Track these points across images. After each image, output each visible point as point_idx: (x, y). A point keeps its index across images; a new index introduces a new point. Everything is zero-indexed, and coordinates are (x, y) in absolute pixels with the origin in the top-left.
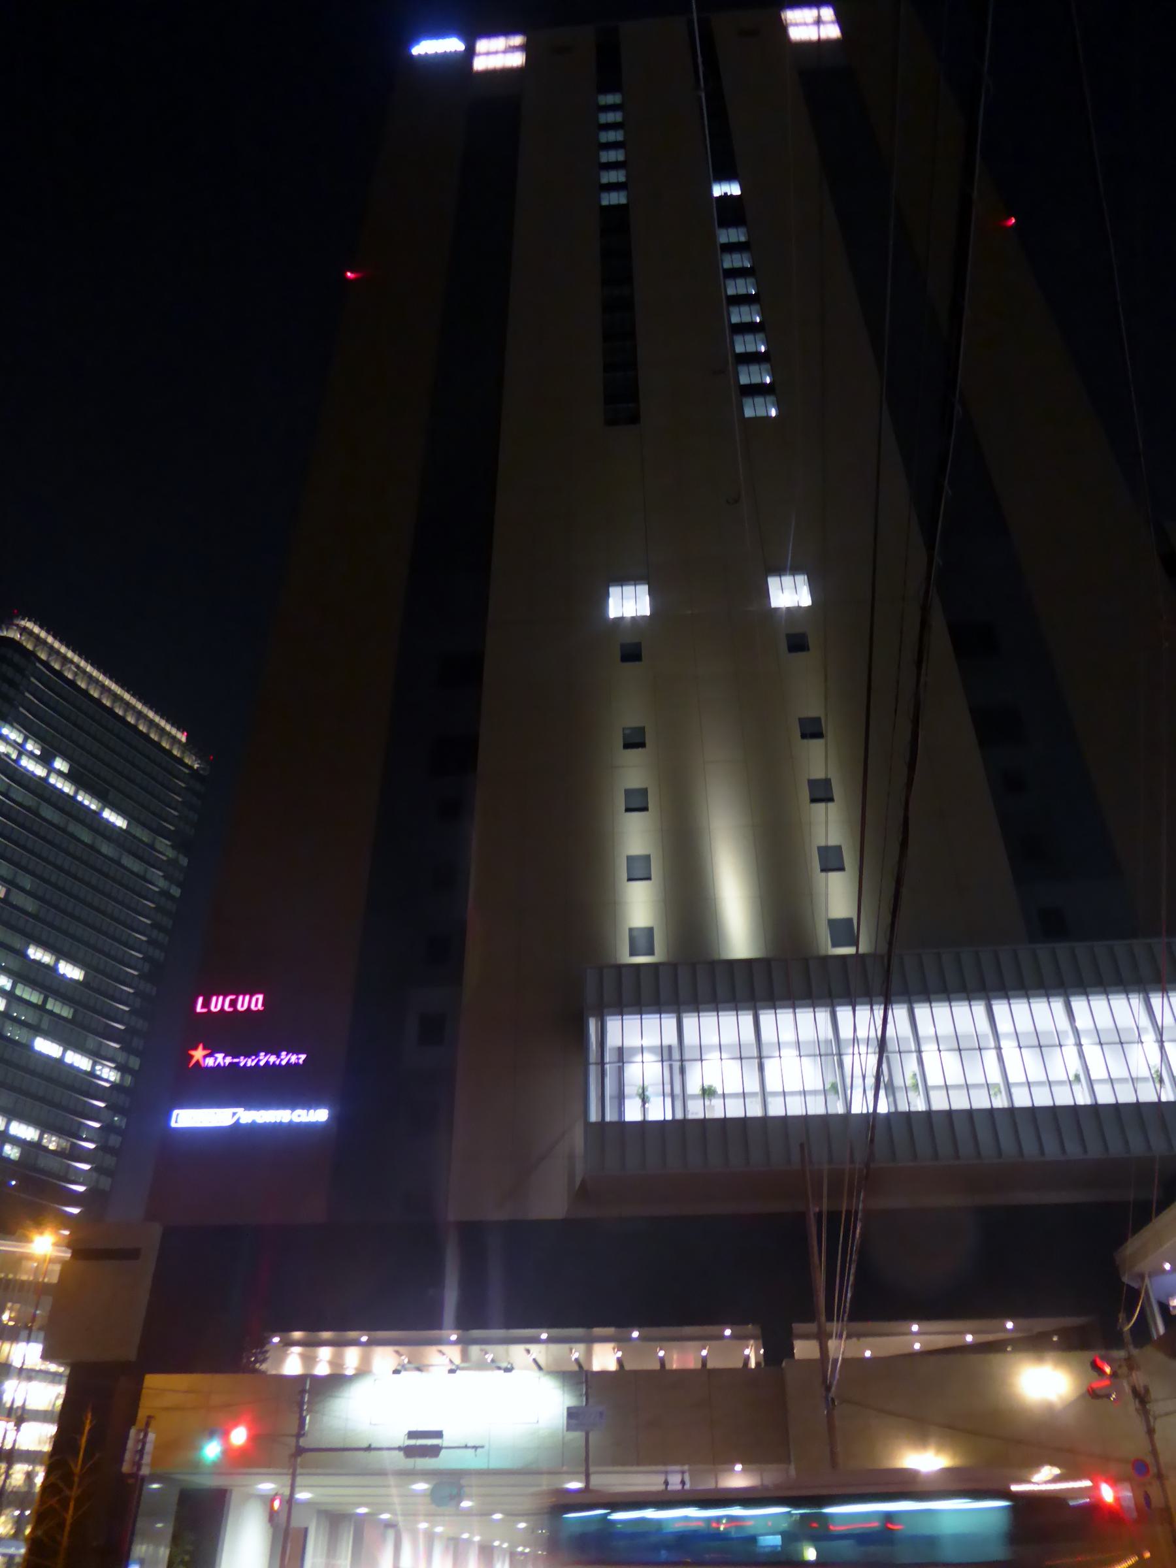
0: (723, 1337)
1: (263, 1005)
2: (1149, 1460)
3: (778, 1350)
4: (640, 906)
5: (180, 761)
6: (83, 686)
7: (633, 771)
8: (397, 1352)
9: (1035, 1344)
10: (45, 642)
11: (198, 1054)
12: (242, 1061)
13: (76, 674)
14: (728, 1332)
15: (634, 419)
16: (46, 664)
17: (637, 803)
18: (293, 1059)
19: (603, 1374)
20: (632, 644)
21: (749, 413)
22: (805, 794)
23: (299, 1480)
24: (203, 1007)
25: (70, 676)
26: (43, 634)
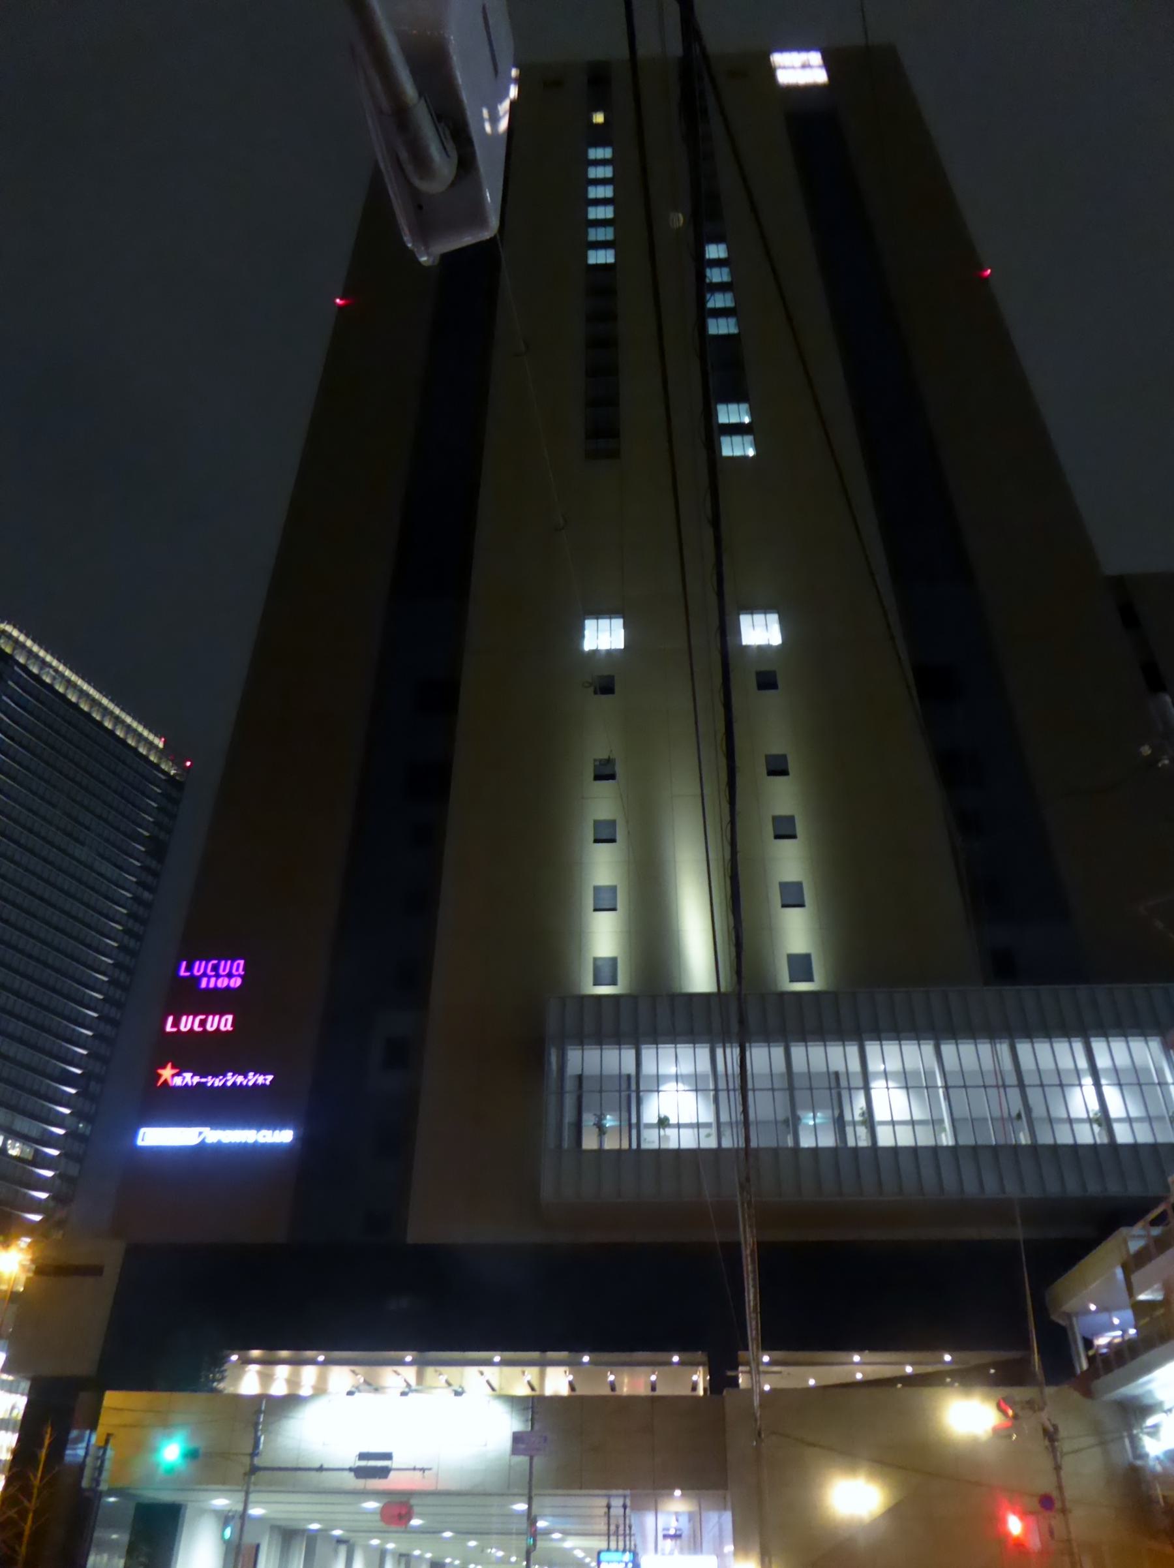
0: (671, 1363)
1: (232, 1025)
2: (1055, 1495)
3: (721, 1381)
4: (604, 937)
5: (157, 767)
6: (61, 690)
7: (602, 803)
8: (353, 1372)
9: (967, 1378)
10: (23, 646)
11: (167, 1073)
12: (210, 1081)
13: (54, 678)
14: (676, 1359)
15: (614, 454)
16: (24, 668)
17: (605, 835)
18: (260, 1080)
19: (556, 1399)
20: (605, 677)
21: (726, 452)
22: (769, 830)
23: (252, 1497)
24: (173, 1026)
25: (48, 680)
26: (22, 638)
